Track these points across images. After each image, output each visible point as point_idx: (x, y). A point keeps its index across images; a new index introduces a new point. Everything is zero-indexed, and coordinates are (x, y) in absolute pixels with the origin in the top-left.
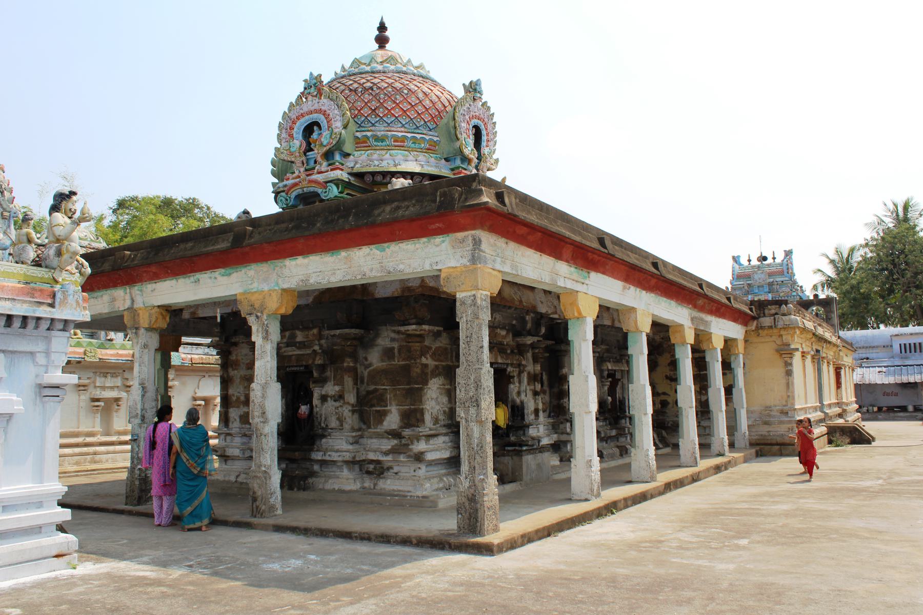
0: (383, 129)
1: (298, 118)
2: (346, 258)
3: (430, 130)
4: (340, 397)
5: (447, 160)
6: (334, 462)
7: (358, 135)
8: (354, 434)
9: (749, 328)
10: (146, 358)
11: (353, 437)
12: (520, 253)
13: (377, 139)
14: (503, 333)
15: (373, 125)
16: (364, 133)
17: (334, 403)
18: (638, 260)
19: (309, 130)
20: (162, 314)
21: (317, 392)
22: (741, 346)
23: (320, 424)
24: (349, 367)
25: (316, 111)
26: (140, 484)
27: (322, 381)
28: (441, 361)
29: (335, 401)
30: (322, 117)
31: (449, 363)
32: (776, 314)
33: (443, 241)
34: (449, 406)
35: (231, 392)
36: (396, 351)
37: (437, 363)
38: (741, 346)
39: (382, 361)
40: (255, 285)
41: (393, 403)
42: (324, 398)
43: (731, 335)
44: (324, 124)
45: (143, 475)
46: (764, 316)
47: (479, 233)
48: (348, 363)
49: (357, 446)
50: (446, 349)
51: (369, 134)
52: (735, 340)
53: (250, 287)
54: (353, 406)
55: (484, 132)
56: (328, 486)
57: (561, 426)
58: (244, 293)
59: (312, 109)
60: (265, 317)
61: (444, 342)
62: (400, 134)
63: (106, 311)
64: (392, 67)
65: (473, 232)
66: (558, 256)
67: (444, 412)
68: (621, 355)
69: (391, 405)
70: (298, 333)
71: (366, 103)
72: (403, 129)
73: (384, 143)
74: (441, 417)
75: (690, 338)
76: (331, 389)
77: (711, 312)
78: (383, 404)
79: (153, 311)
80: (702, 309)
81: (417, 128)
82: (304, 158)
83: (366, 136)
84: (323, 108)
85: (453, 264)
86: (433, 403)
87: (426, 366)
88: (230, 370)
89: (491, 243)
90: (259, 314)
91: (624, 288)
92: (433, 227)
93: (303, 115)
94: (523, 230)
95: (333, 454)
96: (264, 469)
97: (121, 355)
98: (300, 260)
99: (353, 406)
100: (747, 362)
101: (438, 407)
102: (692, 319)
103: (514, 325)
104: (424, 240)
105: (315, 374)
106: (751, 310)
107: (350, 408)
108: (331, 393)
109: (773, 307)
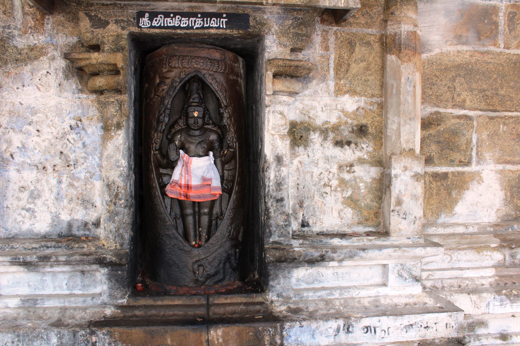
17: (337, 151)
29: (339, 143)
36: (502, 19)
39: (459, 39)
41: (487, 155)
42: (298, 134)
43: (271, 76)
69: (480, 160)
76: (324, 102)
78: (457, 156)
97: (177, 315)
108: (321, 117)
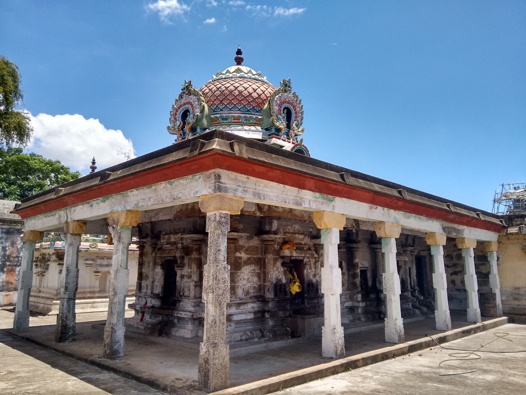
0: (227, 112)
1: (179, 108)
2: (154, 190)
3: (257, 112)
4: (190, 277)
5: (267, 129)
6: (183, 319)
7: (212, 116)
8: (194, 301)
9: (501, 234)
10: (71, 253)
11: (196, 302)
12: (262, 185)
13: (224, 119)
14: (301, 237)
15: (221, 110)
16: (216, 115)
18: (381, 188)
19: (185, 115)
20: (80, 225)
21: (179, 273)
22: (494, 247)
23: (179, 293)
24: (195, 258)
25: (185, 104)
26: (62, 329)
27: (182, 266)
28: (253, 255)
30: (190, 106)
31: (260, 256)
32: (521, 224)
33: (200, 178)
34: (259, 283)
35: (143, 270)
37: (249, 256)
38: (494, 247)
40: (115, 208)
42: (182, 277)
44: (191, 111)
45: (64, 323)
46: (512, 226)
47: (218, 171)
48: (195, 255)
49: (198, 308)
50: (257, 247)
51: (218, 116)
52: (489, 242)
53: (114, 209)
54: (196, 282)
55: (293, 112)
56: (178, 334)
57: (355, 297)
58: (112, 212)
59: (185, 102)
60: (119, 228)
61: (256, 243)
62: (237, 115)
63: (57, 223)
64: (238, 75)
65: (214, 170)
66: (301, 186)
67: (254, 287)
68: (404, 251)
70: (172, 236)
71: (226, 97)
72: (239, 112)
73: (227, 121)
74: (251, 291)
75: (442, 240)
76: (186, 271)
77: (463, 224)
79: (75, 223)
80: (452, 221)
81: (248, 111)
82: (181, 132)
83: (217, 117)
84: (191, 101)
85: (205, 192)
86: (245, 282)
87: (240, 258)
88: (144, 257)
89: (228, 177)
90: (114, 226)
91: (371, 208)
92: (193, 167)
93: (181, 106)
94: (262, 169)
95: (182, 313)
96: (281, 313)
98: (135, 192)
99: (196, 282)
100: (501, 257)
101: (249, 285)
102: (444, 229)
103: (311, 232)
104: (190, 176)
105: (179, 262)
106: (501, 222)
107: (194, 284)
109: (519, 219)
